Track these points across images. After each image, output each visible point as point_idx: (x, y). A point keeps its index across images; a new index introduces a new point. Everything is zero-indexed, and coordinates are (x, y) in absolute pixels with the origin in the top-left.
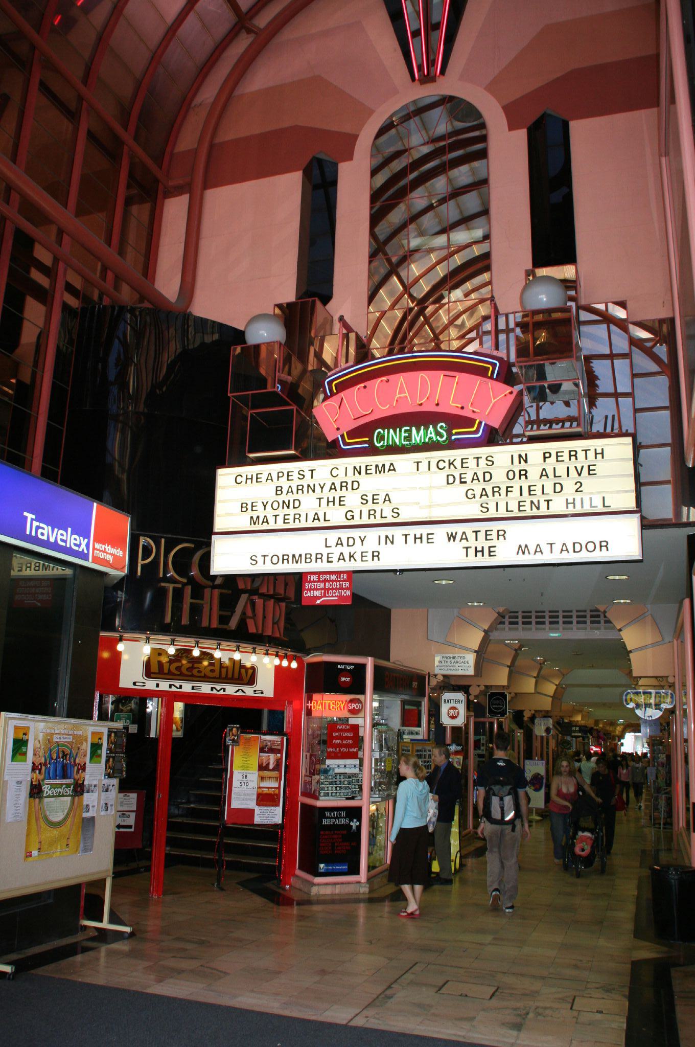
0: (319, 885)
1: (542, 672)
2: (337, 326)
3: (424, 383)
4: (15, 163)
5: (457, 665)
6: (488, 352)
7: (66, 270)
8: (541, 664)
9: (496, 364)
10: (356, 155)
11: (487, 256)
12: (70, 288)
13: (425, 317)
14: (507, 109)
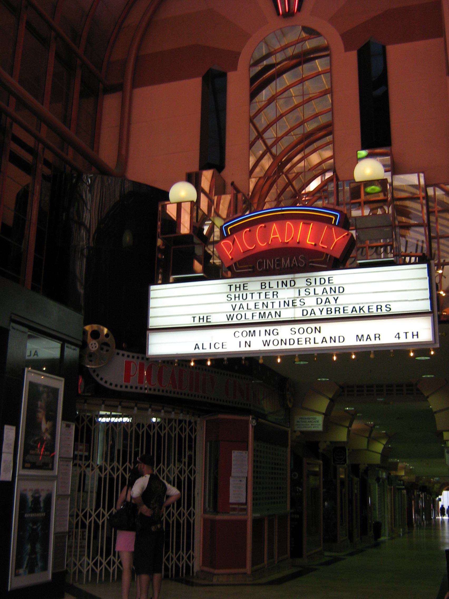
0: (218, 575)
1: (373, 435)
2: (229, 188)
6: (332, 207)
8: (372, 427)
9: (337, 216)
12: (46, 163)
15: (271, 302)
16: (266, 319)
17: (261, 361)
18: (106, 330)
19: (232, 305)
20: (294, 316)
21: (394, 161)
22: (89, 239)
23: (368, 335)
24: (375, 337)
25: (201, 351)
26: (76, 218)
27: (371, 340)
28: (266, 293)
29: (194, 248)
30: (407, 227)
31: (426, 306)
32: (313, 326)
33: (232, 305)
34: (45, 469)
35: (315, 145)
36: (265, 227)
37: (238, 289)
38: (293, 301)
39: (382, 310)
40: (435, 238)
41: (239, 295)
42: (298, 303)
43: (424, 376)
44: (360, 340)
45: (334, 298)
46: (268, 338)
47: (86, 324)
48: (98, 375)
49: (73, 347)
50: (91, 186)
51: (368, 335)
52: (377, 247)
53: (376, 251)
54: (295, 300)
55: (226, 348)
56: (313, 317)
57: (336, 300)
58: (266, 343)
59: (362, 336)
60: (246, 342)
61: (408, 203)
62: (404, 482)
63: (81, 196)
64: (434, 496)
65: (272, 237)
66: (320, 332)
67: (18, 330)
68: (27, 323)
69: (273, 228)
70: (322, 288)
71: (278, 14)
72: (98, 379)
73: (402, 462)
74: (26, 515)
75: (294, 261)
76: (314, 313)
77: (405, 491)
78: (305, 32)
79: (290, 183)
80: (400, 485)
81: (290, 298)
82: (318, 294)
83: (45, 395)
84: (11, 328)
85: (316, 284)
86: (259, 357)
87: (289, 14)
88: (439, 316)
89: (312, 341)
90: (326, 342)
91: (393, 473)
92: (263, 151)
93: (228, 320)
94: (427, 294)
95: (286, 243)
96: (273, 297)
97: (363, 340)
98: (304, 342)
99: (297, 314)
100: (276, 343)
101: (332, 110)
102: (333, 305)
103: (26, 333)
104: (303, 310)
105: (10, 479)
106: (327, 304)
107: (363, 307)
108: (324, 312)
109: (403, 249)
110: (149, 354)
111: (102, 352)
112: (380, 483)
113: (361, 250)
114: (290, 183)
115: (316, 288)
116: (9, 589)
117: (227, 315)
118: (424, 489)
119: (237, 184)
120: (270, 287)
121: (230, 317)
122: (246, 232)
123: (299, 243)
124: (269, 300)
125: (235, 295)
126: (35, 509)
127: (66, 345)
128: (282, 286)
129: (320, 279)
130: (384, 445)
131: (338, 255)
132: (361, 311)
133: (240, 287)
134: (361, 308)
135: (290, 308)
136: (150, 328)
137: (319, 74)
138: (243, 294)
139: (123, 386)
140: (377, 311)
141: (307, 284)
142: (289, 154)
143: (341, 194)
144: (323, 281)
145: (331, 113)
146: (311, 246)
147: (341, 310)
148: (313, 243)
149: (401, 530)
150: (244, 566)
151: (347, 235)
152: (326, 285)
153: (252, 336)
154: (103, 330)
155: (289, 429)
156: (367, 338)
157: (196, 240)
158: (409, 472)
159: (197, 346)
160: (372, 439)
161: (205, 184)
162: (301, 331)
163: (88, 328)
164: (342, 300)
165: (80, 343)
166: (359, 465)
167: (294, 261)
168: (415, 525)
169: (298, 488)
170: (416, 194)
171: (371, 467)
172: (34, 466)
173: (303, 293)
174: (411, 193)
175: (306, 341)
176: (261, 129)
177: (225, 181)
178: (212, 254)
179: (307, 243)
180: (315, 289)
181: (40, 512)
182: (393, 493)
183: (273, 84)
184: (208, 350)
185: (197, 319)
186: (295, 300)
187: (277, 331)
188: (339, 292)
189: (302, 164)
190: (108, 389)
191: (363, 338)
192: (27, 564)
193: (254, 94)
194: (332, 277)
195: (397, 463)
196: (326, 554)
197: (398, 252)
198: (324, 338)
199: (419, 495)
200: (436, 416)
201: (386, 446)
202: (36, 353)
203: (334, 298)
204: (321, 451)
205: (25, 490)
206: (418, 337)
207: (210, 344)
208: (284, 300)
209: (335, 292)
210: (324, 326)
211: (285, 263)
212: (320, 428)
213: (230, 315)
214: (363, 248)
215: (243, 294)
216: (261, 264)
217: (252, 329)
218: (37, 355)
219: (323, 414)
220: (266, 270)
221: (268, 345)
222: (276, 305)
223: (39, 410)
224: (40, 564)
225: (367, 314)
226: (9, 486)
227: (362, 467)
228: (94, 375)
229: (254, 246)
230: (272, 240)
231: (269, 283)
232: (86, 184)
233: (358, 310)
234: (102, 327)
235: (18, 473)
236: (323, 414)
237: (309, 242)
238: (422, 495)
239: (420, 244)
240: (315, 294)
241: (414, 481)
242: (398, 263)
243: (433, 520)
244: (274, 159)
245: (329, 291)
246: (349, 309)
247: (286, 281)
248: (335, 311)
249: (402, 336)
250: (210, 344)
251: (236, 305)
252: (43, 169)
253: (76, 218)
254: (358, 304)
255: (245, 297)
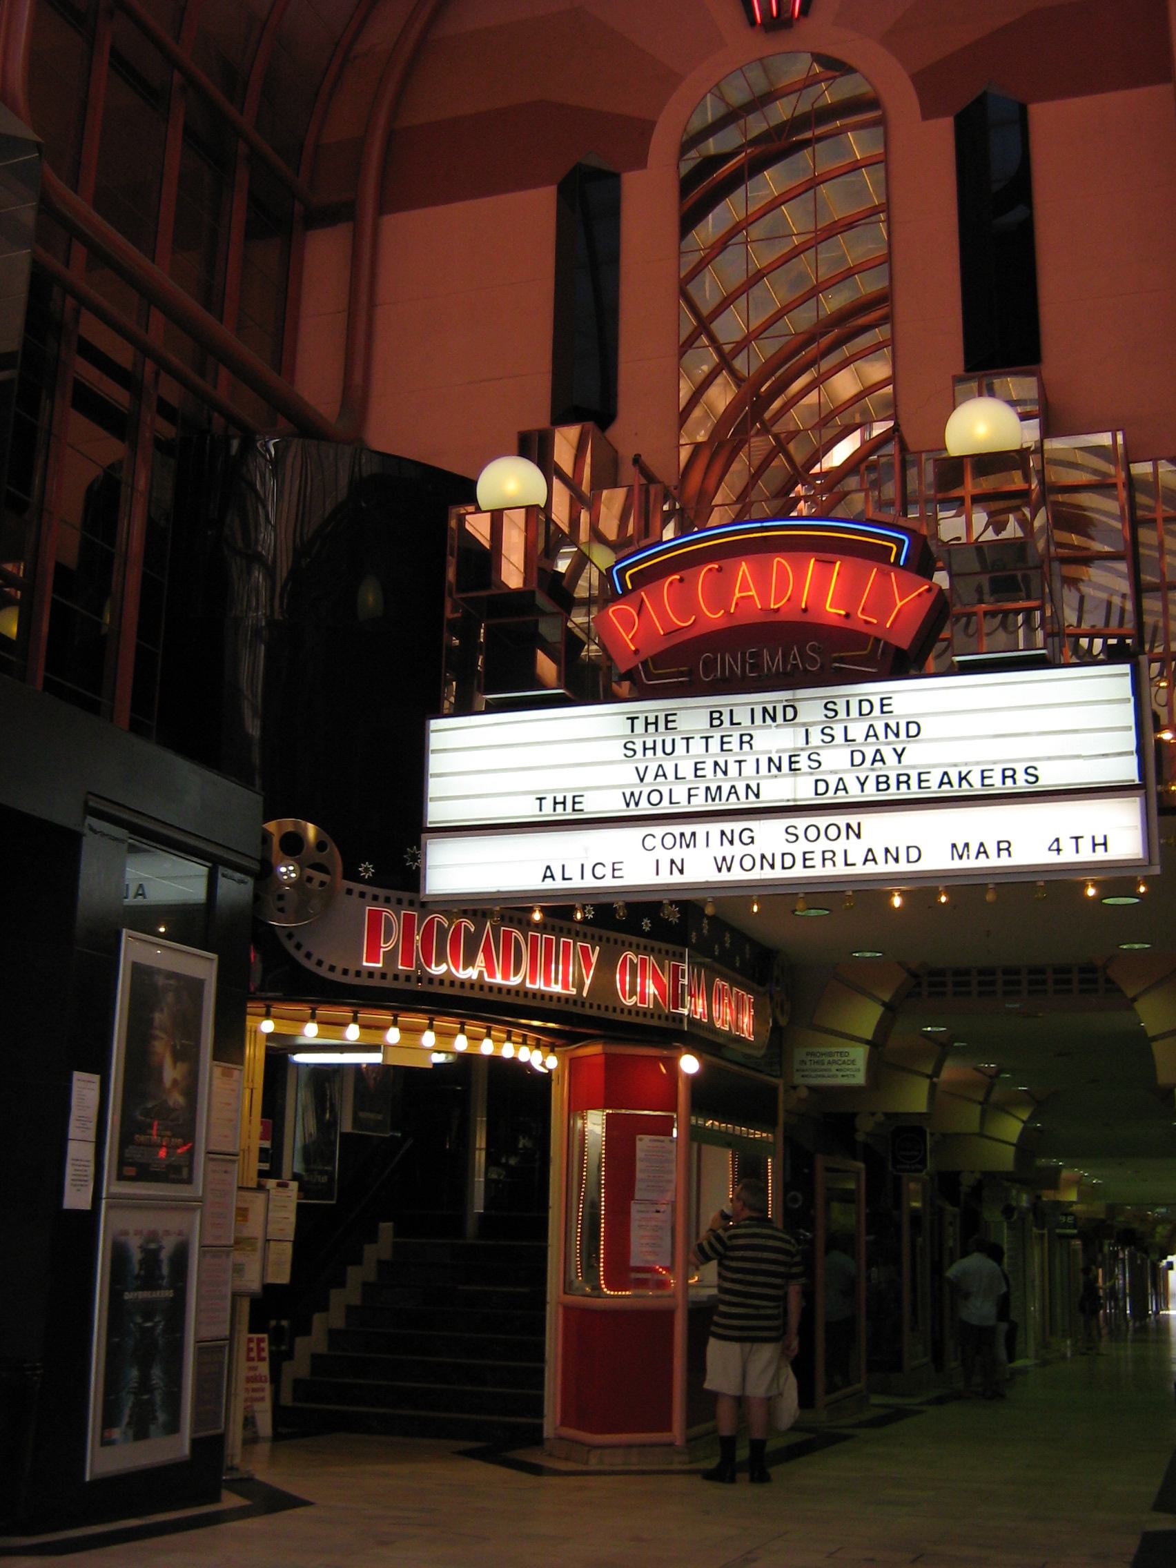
1: (995, 1096)
2: (629, 473)
3: (782, 570)
4: (76, 192)
5: (835, 1067)
7: (157, 375)
9: (903, 541)
10: (652, 159)
11: (883, 299)
12: (165, 409)
13: (762, 423)
14: (921, 80)
15: (736, 761)
16: (723, 804)
17: (709, 910)
18: (311, 830)
19: (637, 769)
20: (792, 797)
21: (1046, 399)
22: (272, 599)
23: (982, 845)
24: (999, 850)
25: (559, 884)
26: (240, 544)
27: (987, 857)
28: (722, 737)
29: (536, 623)
30: (1087, 559)
31: (1127, 770)
32: (842, 820)
33: (637, 769)
34: (174, 1181)
35: (846, 351)
36: (720, 570)
37: (651, 728)
38: (790, 757)
39: (1017, 782)
40: (1154, 588)
41: (655, 742)
42: (803, 763)
43: (1125, 947)
44: (961, 857)
45: (895, 750)
46: (727, 850)
47: (267, 820)
48: (298, 946)
49: (238, 875)
50: (277, 463)
51: (982, 845)
52: (1006, 613)
53: (1004, 625)
54: (795, 756)
55: (622, 877)
56: (842, 798)
57: (900, 756)
58: (723, 864)
59: (967, 845)
60: (672, 862)
61: (1085, 499)
62: (1075, 1220)
63: (252, 486)
64: (1155, 1257)
65: (737, 595)
66: (858, 836)
67: (103, 835)
68: (125, 816)
69: (741, 573)
70: (865, 725)
71: (753, 22)
72: (299, 956)
73: (1073, 1167)
74: (128, 1296)
75: (795, 656)
76: (845, 789)
77: (1077, 1243)
78: (820, 64)
79: (781, 447)
80: (1066, 1226)
81: (784, 751)
82: (854, 740)
83: (170, 998)
84: (86, 831)
85: (848, 714)
86: (705, 902)
87: (778, 23)
88: (1160, 795)
89: (839, 859)
90: (876, 863)
91: (1048, 1196)
92: (712, 365)
93: (628, 805)
94: (1129, 741)
95: (773, 609)
96: (741, 748)
97: (968, 857)
98: (817, 861)
99: (801, 790)
100: (748, 863)
101: (888, 259)
102: (891, 768)
103: (122, 841)
104: (817, 781)
105: (88, 1207)
106: (877, 765)
107: (969, 772)
108: (870, 786)
109: (1070, 617)
110: (427, 892)
111: (309, 885)
112: (1013, 1220)
113: (964, 620)
114: (781, 447)
115: (850, 726)
116: (88, 1479)
117: (624, 794)
118: (1129, 1237)
119: (649, 461)
120: (732, 723)
121: (631, 799)
122: (671, 583)
123: (805, 610)
124: (732, 756)
125: (644, 742)
126: (149, 1279)
127: (221, 870)
128: (764, 721)
129: (860, 701)
130: (1023, 1122)
131: (904, 641)
132: (964, 782)
133: (656, 723)
134: (963, 775)
135: (785, 775)
136: (429, 826)
137: (855, 167)
138: (664, 741)
139: (324, 964)
140: (1004, 783)
141: (826, 716)
142: (778, 374)
143: (912, 472)
144: (866, 707)
145: (886, 266)
146: (837, 617)
147: (914, 782)
148: (843, 612)
149: (1068, 1342)
150: (668, 1427)
151: (929, 590)
152: (876, 718)
153: (688, 846)
154: (305, 830)
155: (779, 1082)
156: (979, 852)
157: (542, 600)
158: (1088, 1193)
159: (548, 874)
160: (992, 1108)
161: (563, 453)
162: (812, 833)
163: (271, 826)
164: (916, 755)
165: (255, 866)
166: (958, 1174)
167: (795, 658)
168: (1104, 1332)
169: (801, 1231)
170: (1110, 476)
171: (991, 1179)
172: (145, 1174)
173: (816, 738)
174: (1095, 472)
175: (824, 860)
176: (705, 311)
177: (617, 452)
178: (582, 636)
179: (827, 611)
180: (846, 728)
181: (160, 1288)
182: (1046, 1245)
183: (740, 193)
184: (577, 883)
185: (547, 805)
186: (795, 756)
187: (751, 834)
188: (908, 736)
189: (813, 397)
190: (324, 980)
191: (968, 851)
192: (131, 1417)
193: (690, 220)
194: (890, 698)
195: (1058, 1170)
196: (875, 1399)
197: (1056, 626)
198: (870, 850)
199: (1117, 1253)
200: (1156, 1047)
201: (1029, 1125)
202: (141, 891)
203: (895, 750)
204: (860, 1137)
205: (126, 1233)
206: (1106, 850)
207: (582, 865)
208: (770, 755)
209: (897, 735)
210: (869, 821)
211: (772, 662)
212: (860, 1079)
213: (632, 794)
214: (969, 616)
215: (664, 741)
216: (710, 665)
217: (687, 829)
218: (143, 895)
219: (867, 1042)
220: (724, 680)
221: (729, 869)
222: (749, 769)
223: (158, 1033)
224: (161, 1417)
225: (978, 789)
226: (88, 1219)
227: (967, 1181)
228: (289, 946)
229: (693, 617)
230: (737, 604)
231: (731, 711)
232: (264, 457)
233: (955, 781)
234: (303, 822)
235: (107, 1191)
236: (867, 1042)
237: (832, 609)
238: (1124, 1254)
239: (1117, 600)
240: (846, 740)
241: (1102, 1216)
242: (1057, 662)
243: (1152, 1317)
244: (738, 386)
245: (881, 733)
246: (934, 779)
247: (774, 708)
248: (899, 782)
249: (1067, 845)
250: (582, 865)
251: (647, 768)
252: (156, 426)
253: (240, 544)
254: (955, 765)
255: (668, 749)
